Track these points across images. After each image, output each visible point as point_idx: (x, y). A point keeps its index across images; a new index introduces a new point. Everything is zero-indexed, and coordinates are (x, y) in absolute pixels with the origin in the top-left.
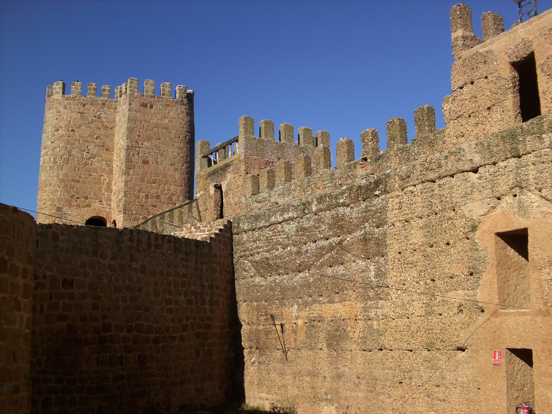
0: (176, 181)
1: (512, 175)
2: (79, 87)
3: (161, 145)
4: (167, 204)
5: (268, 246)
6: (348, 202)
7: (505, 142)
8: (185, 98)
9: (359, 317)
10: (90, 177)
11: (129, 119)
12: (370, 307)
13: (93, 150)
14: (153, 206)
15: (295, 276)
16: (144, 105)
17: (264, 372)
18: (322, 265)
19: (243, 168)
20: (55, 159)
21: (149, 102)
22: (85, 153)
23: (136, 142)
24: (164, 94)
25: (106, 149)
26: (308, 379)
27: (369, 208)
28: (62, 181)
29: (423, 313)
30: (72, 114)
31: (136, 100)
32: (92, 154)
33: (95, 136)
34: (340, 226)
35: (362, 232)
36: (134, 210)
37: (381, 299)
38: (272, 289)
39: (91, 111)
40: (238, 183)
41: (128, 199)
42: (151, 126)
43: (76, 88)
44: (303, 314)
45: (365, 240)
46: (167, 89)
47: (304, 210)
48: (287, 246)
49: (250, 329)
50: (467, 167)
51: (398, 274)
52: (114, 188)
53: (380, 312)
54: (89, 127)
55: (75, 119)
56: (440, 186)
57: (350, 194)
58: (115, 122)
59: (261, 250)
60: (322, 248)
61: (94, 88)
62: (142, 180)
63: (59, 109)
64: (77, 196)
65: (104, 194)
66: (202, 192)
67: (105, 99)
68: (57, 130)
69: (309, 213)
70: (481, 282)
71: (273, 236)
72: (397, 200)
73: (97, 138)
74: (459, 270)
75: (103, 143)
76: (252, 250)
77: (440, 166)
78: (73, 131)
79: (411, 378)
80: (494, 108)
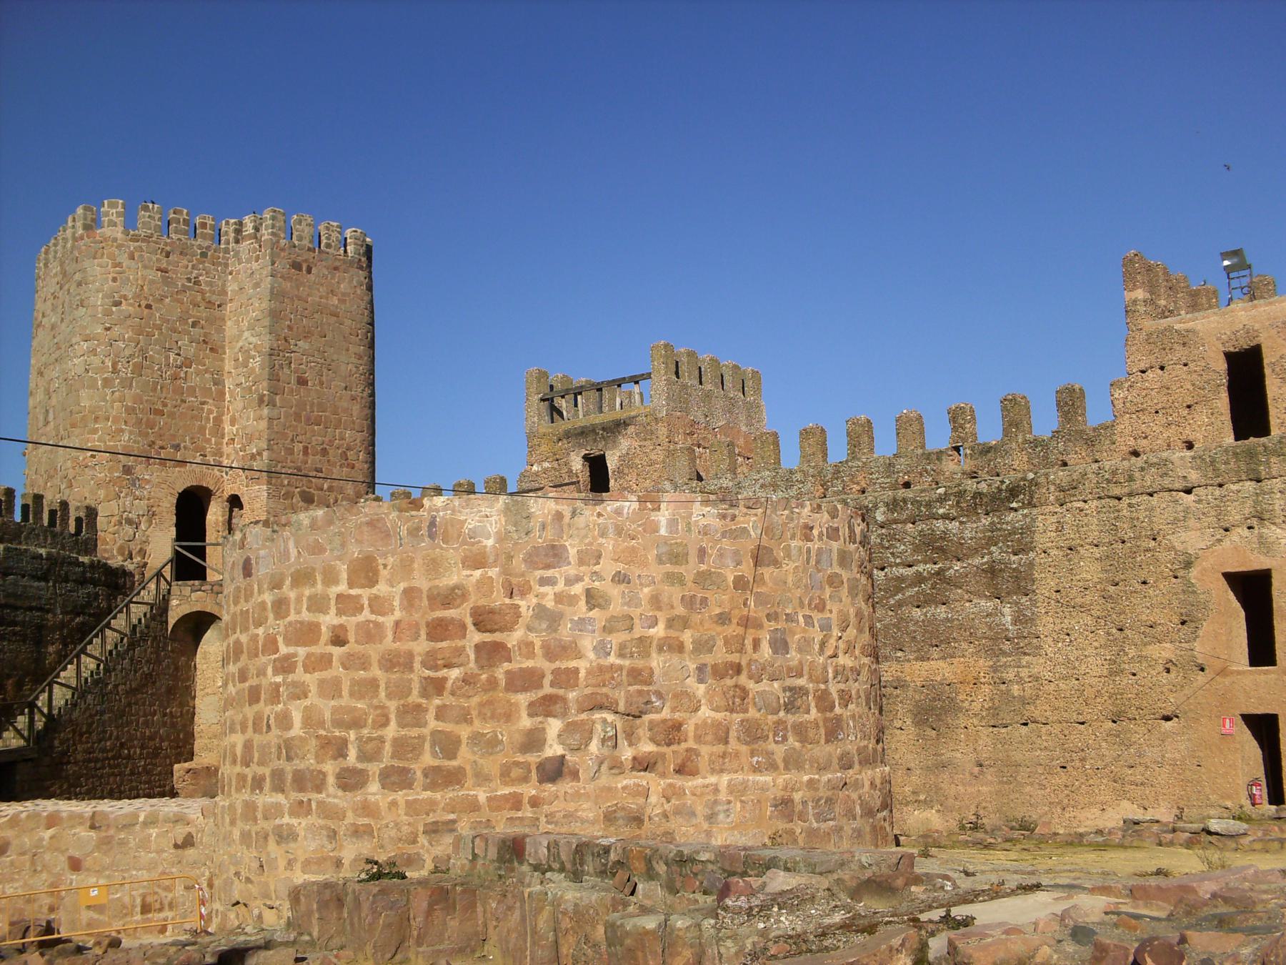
0: (354, 422)
1: (1250, 503)
2: (157, 216)
6: (954, 512)
7: (1238, 460)
9: (983, 680)
11: (272, 293)
12: (1005, 666)
18: (900, 604)
19: (662, 431)
20: (114, 365)
21: (306, 261)
22: (172, 356)
25: (211, 349)
28: (130, 411)
29: (1105, 673)
33: (190, 321)
34: (935, 546)
37: (1025, 654)
39: (182, 268)
40: (653, 457)
41: (274, 456)
45: (992, 571)
46: (335, 235)
50: (1177, 486)
51: (1058, 621)
52: (227, 428)
53: (1024, 673)
54: (178, 301)
55: (152, 282)
56: (1130, 505)
57: (958, 502)
60: (901, 579)
62: (297, 417)
64: (159, 443)
66: (546, 465)
67: (207, 243)
70: (1200, 633)
72: (1054, 519)
73: (194, 325)
74: (1167, 619)
75: (205, 335)
77: (1131, 479)
78: (149, 307)
79: (1083, 760)
80: (1198, 407)
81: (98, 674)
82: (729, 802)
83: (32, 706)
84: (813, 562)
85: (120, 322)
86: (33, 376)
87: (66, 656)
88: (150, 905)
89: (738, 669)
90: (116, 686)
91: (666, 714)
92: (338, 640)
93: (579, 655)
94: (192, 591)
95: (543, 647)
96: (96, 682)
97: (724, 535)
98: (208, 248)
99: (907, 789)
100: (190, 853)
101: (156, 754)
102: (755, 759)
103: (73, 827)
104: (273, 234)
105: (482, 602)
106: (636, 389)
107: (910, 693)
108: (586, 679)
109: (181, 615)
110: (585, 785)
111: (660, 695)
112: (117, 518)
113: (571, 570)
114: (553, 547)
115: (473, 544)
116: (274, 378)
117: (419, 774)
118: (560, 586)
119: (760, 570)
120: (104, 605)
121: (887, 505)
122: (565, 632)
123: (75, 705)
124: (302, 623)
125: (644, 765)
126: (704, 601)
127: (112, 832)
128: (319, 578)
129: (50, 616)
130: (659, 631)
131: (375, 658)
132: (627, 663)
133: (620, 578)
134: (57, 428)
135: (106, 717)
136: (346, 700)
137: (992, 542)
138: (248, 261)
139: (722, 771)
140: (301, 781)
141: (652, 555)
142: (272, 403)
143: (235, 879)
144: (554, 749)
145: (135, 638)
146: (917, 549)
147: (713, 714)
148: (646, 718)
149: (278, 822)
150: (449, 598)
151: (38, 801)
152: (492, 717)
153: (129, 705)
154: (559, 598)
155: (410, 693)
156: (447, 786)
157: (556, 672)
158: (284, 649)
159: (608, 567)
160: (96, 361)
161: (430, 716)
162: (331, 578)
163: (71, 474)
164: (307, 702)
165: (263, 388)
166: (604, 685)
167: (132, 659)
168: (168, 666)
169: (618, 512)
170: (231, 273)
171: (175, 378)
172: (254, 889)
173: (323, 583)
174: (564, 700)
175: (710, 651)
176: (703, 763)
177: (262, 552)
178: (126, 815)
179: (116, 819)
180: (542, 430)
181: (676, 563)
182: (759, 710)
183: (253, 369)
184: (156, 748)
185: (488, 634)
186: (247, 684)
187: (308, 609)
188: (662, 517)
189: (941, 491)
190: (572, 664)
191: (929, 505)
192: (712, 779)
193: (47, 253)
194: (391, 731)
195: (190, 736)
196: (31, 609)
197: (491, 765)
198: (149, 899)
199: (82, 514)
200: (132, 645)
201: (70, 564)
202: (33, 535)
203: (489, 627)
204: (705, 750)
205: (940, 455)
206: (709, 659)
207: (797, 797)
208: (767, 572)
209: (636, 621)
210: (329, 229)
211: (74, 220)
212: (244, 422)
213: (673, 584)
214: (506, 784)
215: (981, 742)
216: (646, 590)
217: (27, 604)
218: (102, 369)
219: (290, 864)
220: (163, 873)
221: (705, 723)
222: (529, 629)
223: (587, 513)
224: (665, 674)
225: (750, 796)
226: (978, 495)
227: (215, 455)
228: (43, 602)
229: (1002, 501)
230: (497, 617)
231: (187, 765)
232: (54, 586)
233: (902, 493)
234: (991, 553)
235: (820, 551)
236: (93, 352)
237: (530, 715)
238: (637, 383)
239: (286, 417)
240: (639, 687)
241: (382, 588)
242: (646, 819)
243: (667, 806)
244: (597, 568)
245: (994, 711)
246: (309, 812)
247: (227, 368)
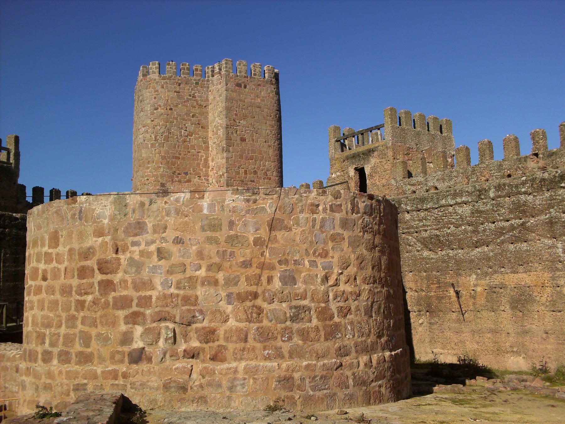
2: (174, 67)
3: (255, 123)
4: (264, 179)
5: (438, 225)
6: (530, 190)
8: (273, 78)
9: (547, 285)
11: (226, 99)
13: (192, 128)
14: (251, 181)
15: (472, 250)
16: (239, 85)
17: (437, 332)
18: (503, 242)
19: (390, 153)
21: (243, 82)
22: (183, 131)
24: (255, 75)
25: (202, 127)
26: (489, 335)
27: (554, 197)
28: (163, 158)
30: (168, 93)
31: (231, 80)
33: (191, 115)
34: (521, 210)
35: (547, 217)
38: (444, 261)
39: (186, 90)
40: (386, 167)
41: (230, 176)
42: (246, 105)
43: (170, 68)
44: (483, 282)
45: (551, 223)
46: (258, 70)
47: (480, 195)
48: (460, 225)
49: (418, 296)
52: (211, 164)
54: (184, 105)
55: (172, 98)
57: (532, 185)
58: (208, 101)
59: (429, 228)
60: (503, 228)
61: (187, 68)
62: (241, 157)
66: (338, 174)
67: (199, 78)
69: (486, 199)
71: (444, 216)
73: (193, 116)
76: (417, 228)
78: (171, 109)
82: (245, 379)
84: (317, 227)
89: (255, 296)
91: (205, 324)
93: (153, 288)
95: (132, 283)
97: (248, 212)
98: (199, 80)
99: (507, 344)
102: (266, 352)
104: (226, 71)
105: (102, 256)
106: (379, 132)
107: (508, 291)
108: (156, 302)
110: (155, 366)
111: (201, 312)
113: (149, 237)
114: (139, 223)
115: (99, 222)
116: (228, 138)
117: (74, 356)
118: (143, 247)
119: (274, 233)
121: (495, 187)
122: (145, 274)
125: (192, 355)
126: (232, 254)
130: (202, 273)
131: (57, 288)
132: (182, 292)
133: (178, 241)
137: (551, 206)
138: (217, 85)
139: (241, 359)
141: (198, 227)
142: (228, 151)
144: (138, 344)
146: (511, 211)
147: (237, 324)
148: (194, 326)
150: (87, 254)
152: (106, 324)
154: (142, 253)
155: (70, 309)
156: (85, 363)
157: (140, 298)
159: (170, 234)
160: (148, 136)
161: (79, 322)
165: (224, 144)
166: (167, 306)
169: (177, 200)
174: (144, 315)
175: (236, 284)
176: (229, 354)
180: (336, 156)
181: (214, 231)
182: (271, 321)
183: (220, 135)
185: (105, 275)
188: (205, 203)
189: (524, 178)
190: (149, 293)
191: (517, 187)
192: (234, 365)
194: (63, 330)
197: (106, 352)
203: (105, 271)
204: (231, 346)
205: (526, 158)
206: (235, 290)
207: (297, 375)
208: (279, 235)
209: (188, 267)
210: (255, 67)
213: (211, 244)
214: (112, 363)
215: (546, 320)
216: (194, 248)
218: (150, 140)
221: (231, 330)
222: (125, 272)
223: (159, 202)
224: (206, 299)
225: (260, 376)
226: (543, 180)
229: (556, 183)
230: (109, 265)
233: (507, 181)
234: (550, 213)
235: (323, 220)
237: (126, 323)
238: (379, 129)
239: (235, 157)
240: (188, 307)
241: (60, 249)
242: (189, 388)
243: (203, 381)
244: (164, 235)
245: (553, 303)
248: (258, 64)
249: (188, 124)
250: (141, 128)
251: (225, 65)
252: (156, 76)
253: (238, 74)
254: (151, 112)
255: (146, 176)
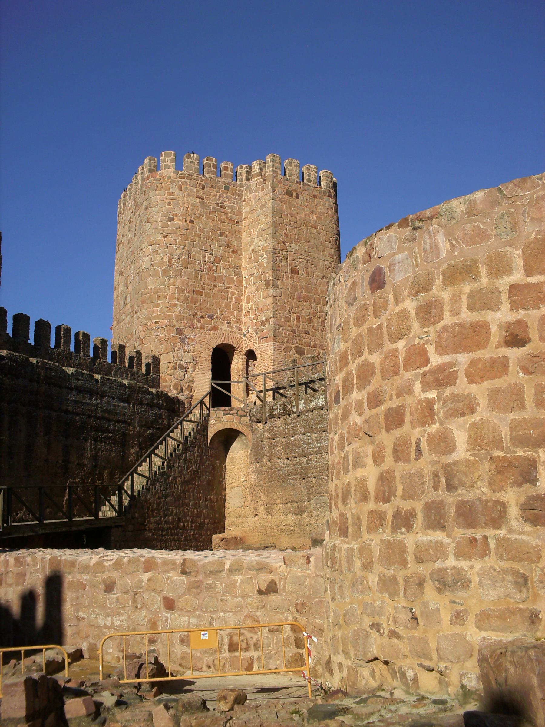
2: (196, 162)
3: (310, 250)
4: (321, 330)
10: (215, 288)
11: (273, 211)
13: (219, 252)
21: (295, 190)
22: (207, 255)
23: (284, 243)
24: (309, 181)
25: (233, 252)
32: (216, 257)
33: (219, 232)
36: (285, 337)
39: (213, 197)
41: (278, 322)
52: (244, 304)
55: (193, 205)
58: (241, 214)
61: (214, 164)
63: (171, 191)
64: (200, 314)
65: (232, 313)
67: (228, 180)
68: (171, 220)
73: (221, 235)
78: (192, 222)
81: (163, 468)
83: (121, 488)
85: (174, 232)
86: (116, 274)
87: (141, 456)
88: (237, 644)
90: (175, 478)
92: (516, 338)
94: (224, 414)
96: (162, 474)
98: (229, 184)
100: (273, 598)
101: (201, 526)
103: (166, 571)
104: (273, 171)
109: (217, 431)
112: (173, 364)
116: (276, 269)
120: (165, 422)
123: (148, 489)
124: (461, 325)
127: (200, 577)
128: (483, 270)
129: (131, 428)
134: (132, 307)
135: (169, 499)
136: (530, 411)
138: (256, 191)
140: (468, 515)
142: (275, 286)
143: (374, 633)
145: (187, 445)
149: (438, 564)
151: (135, 550)
153: (184, 492)
158: (436, 359)
160: (158, 258)
162: (499, 266)
163: (142, 335)
164: (476, 418)
165: (269, 275)
167: (185, 460)
168: (208, 466)
170: (244, 201)
171: (210, 270)
172: (402, 646)
173: (490, 274)
177: (399, 257)
178: (213, 563)
179: (204, 566)
183: (262, 263)
184: (201, 523)
186: (382, 409)
187: (471, 308)
193: (124, 196)
195: (223, 516)
196: (119, 421)
198: (236, 639)
199: (150, 361)
200: (185, 450)
201: (144, 392)
202: (120, 372)
207: (447, 439)
210: (310, 171)
211: (143, 169)
212: (256, 300)
217: (116, 418)
219: (458, 617)
220: (248, 616)
227: (237, 323)
228: (126, 417)
231: (221, 536)
232: (133, 407)
236: (156, 252)
239: (285, 295)
246: (485, 552)
247: (243, 265)
248: (313, 166)
249: (215, 246)
250: (146, 247)
251: (271, 163)
252: (171, 172)
253: (288, 178)
254: (163, 224)
255: (154, 317)
